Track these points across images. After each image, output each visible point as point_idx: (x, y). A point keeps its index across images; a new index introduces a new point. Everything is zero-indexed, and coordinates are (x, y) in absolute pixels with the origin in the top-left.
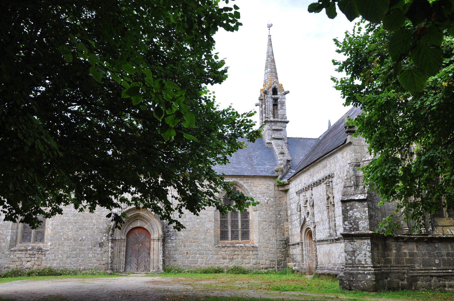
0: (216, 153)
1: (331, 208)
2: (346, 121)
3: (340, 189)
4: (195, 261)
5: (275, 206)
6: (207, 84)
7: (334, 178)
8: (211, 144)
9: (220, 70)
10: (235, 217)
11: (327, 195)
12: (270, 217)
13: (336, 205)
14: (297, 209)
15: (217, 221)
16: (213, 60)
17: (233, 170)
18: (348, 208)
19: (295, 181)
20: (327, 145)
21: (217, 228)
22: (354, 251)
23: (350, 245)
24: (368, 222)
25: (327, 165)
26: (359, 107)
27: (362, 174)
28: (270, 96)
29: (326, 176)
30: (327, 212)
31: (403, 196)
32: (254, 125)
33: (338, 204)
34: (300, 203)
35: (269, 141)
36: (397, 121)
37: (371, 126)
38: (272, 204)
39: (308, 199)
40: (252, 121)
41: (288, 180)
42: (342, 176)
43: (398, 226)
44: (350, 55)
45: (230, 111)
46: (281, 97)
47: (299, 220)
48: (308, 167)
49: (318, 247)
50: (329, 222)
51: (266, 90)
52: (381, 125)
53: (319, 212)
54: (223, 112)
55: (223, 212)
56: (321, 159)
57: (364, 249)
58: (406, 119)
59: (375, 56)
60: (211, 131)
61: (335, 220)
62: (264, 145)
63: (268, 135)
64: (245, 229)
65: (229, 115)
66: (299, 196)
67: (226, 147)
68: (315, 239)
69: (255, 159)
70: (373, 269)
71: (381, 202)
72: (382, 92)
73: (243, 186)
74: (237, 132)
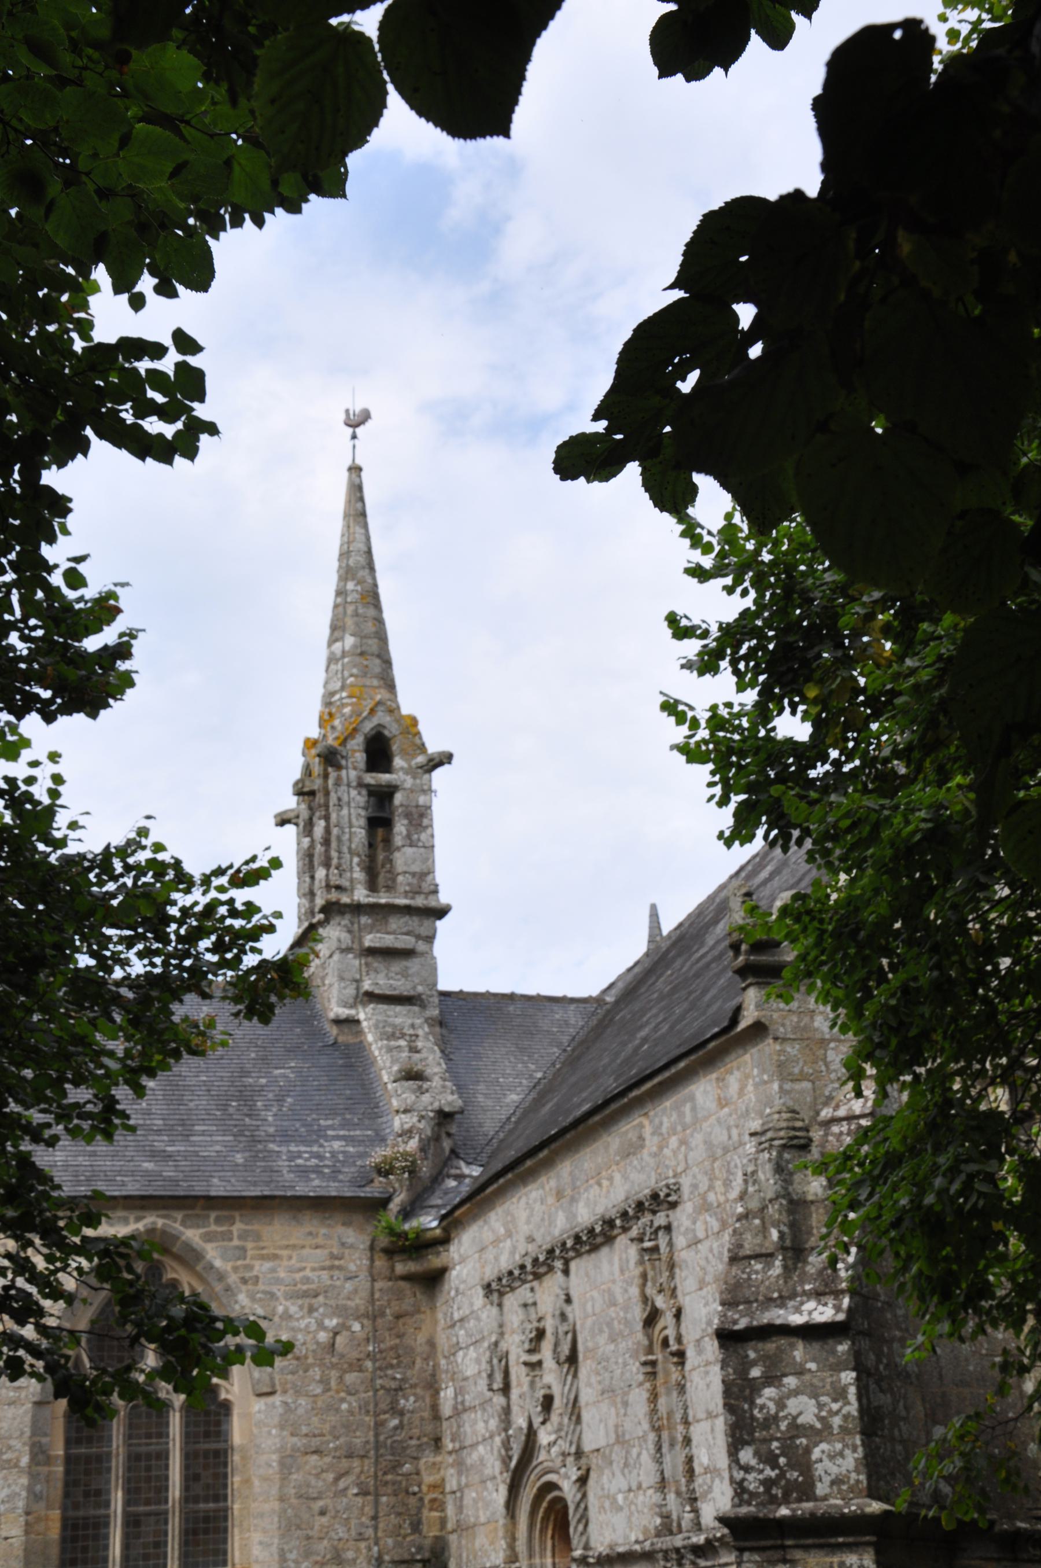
0: (62, 1080)
1: (667, 1374)
2: (738, 916)
3: (710, 1269)
5: (374, 1360)
6: (20, 717)
7: (679, 1209)
8: (33, 1029)
9: (92, 644)
10: (149, 1436)
11: (645, 1299)
12: (347, 1426)
13: (690, 1353)
14: (490, 1376)
15: (49, 1460)
16: (52, 592)
17: (148, 1166)
18: (755, 1372)
19: (480, 1223)
20: (643, 1033)
21: (42, 1504)
24: (860, 1453)
25: (641, 1138)
26: (797, 854)
27: (820, 1191)
28: (353, 774)
29: (640, 1196)
30: (645, 1395)
31: (1029, 1307)
32: (271, 929)
33: (700, 1351)
34: (503, 1346)
35: (344, 1012)
36: (986, 924)
37: (860, 947)
38: (355, 1355)
39: (549, 1325)
40: (258, 910)
41: (443, 1218)
42: (722, 1199)
43: (1009, 1474)
44: (753, 594)
45: (142, 857)
46: (409, 782)
47: (498, 1440)
48: (545, 1153)
50: (659, 1449)
51: (336, 744)
52: (910, 943)
53: (607, 1392)
54: (104, 860)
55: (89, 1411)
56: (614, 1106)
58: (1032, 914)
59: (875, 602)
60: (38, 962)
61: (687, 1441)
62: (319, 1034)
63: (342, 979)
64: (206, 1500)
65: (136, 879)
66: (500, 1305)
67: (118, 1046)
68: (587, 1547)
69: (267, 1108)
71: (920, 1338)
72: (908, 781)
73: (198, 1256)
74: (176, 967)
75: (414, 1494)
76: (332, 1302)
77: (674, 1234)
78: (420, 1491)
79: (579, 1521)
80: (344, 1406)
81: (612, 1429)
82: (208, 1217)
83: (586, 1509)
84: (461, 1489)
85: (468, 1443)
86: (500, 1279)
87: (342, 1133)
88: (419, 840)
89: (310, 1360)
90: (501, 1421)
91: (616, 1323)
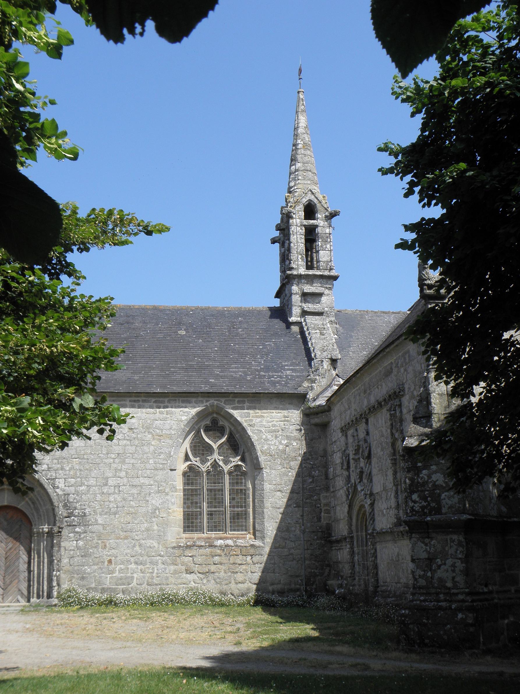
4: (127, 578)
22: (430, 560)
23: (423, 545)
28: (298, 221)
29: (390, 393)
34: (347, 452)
38: (294, 454)
47: (345, 488)
49: (378, 547)
57: (451, 555)
64: (238, 507)
68: (374, 529)
70: (469, 598)
75: (318, 507)
76: (285, 434)
77: (402, 408)
78: (321, 506)
79: (371, 520)
80: (290, 474)
81: (382, 485)
82: (235, 400)
83: (374, 515)
84: (335, 506)
85: (337, 489)
86: (345, 426)
87: (291, 368)
88: (326, 247)
89: (276, 456)
90: (346, 481)
91: (383, 443)
